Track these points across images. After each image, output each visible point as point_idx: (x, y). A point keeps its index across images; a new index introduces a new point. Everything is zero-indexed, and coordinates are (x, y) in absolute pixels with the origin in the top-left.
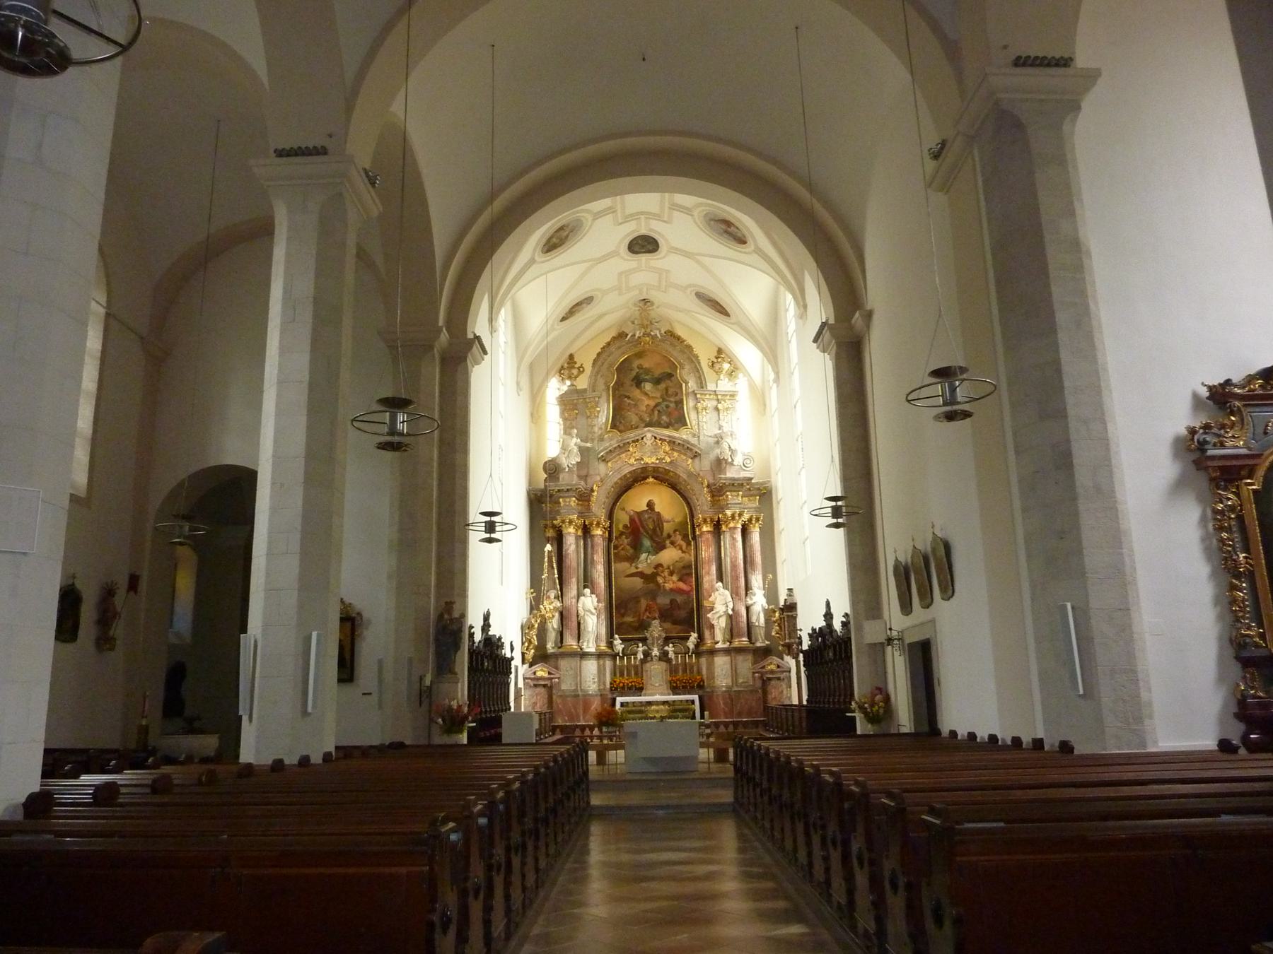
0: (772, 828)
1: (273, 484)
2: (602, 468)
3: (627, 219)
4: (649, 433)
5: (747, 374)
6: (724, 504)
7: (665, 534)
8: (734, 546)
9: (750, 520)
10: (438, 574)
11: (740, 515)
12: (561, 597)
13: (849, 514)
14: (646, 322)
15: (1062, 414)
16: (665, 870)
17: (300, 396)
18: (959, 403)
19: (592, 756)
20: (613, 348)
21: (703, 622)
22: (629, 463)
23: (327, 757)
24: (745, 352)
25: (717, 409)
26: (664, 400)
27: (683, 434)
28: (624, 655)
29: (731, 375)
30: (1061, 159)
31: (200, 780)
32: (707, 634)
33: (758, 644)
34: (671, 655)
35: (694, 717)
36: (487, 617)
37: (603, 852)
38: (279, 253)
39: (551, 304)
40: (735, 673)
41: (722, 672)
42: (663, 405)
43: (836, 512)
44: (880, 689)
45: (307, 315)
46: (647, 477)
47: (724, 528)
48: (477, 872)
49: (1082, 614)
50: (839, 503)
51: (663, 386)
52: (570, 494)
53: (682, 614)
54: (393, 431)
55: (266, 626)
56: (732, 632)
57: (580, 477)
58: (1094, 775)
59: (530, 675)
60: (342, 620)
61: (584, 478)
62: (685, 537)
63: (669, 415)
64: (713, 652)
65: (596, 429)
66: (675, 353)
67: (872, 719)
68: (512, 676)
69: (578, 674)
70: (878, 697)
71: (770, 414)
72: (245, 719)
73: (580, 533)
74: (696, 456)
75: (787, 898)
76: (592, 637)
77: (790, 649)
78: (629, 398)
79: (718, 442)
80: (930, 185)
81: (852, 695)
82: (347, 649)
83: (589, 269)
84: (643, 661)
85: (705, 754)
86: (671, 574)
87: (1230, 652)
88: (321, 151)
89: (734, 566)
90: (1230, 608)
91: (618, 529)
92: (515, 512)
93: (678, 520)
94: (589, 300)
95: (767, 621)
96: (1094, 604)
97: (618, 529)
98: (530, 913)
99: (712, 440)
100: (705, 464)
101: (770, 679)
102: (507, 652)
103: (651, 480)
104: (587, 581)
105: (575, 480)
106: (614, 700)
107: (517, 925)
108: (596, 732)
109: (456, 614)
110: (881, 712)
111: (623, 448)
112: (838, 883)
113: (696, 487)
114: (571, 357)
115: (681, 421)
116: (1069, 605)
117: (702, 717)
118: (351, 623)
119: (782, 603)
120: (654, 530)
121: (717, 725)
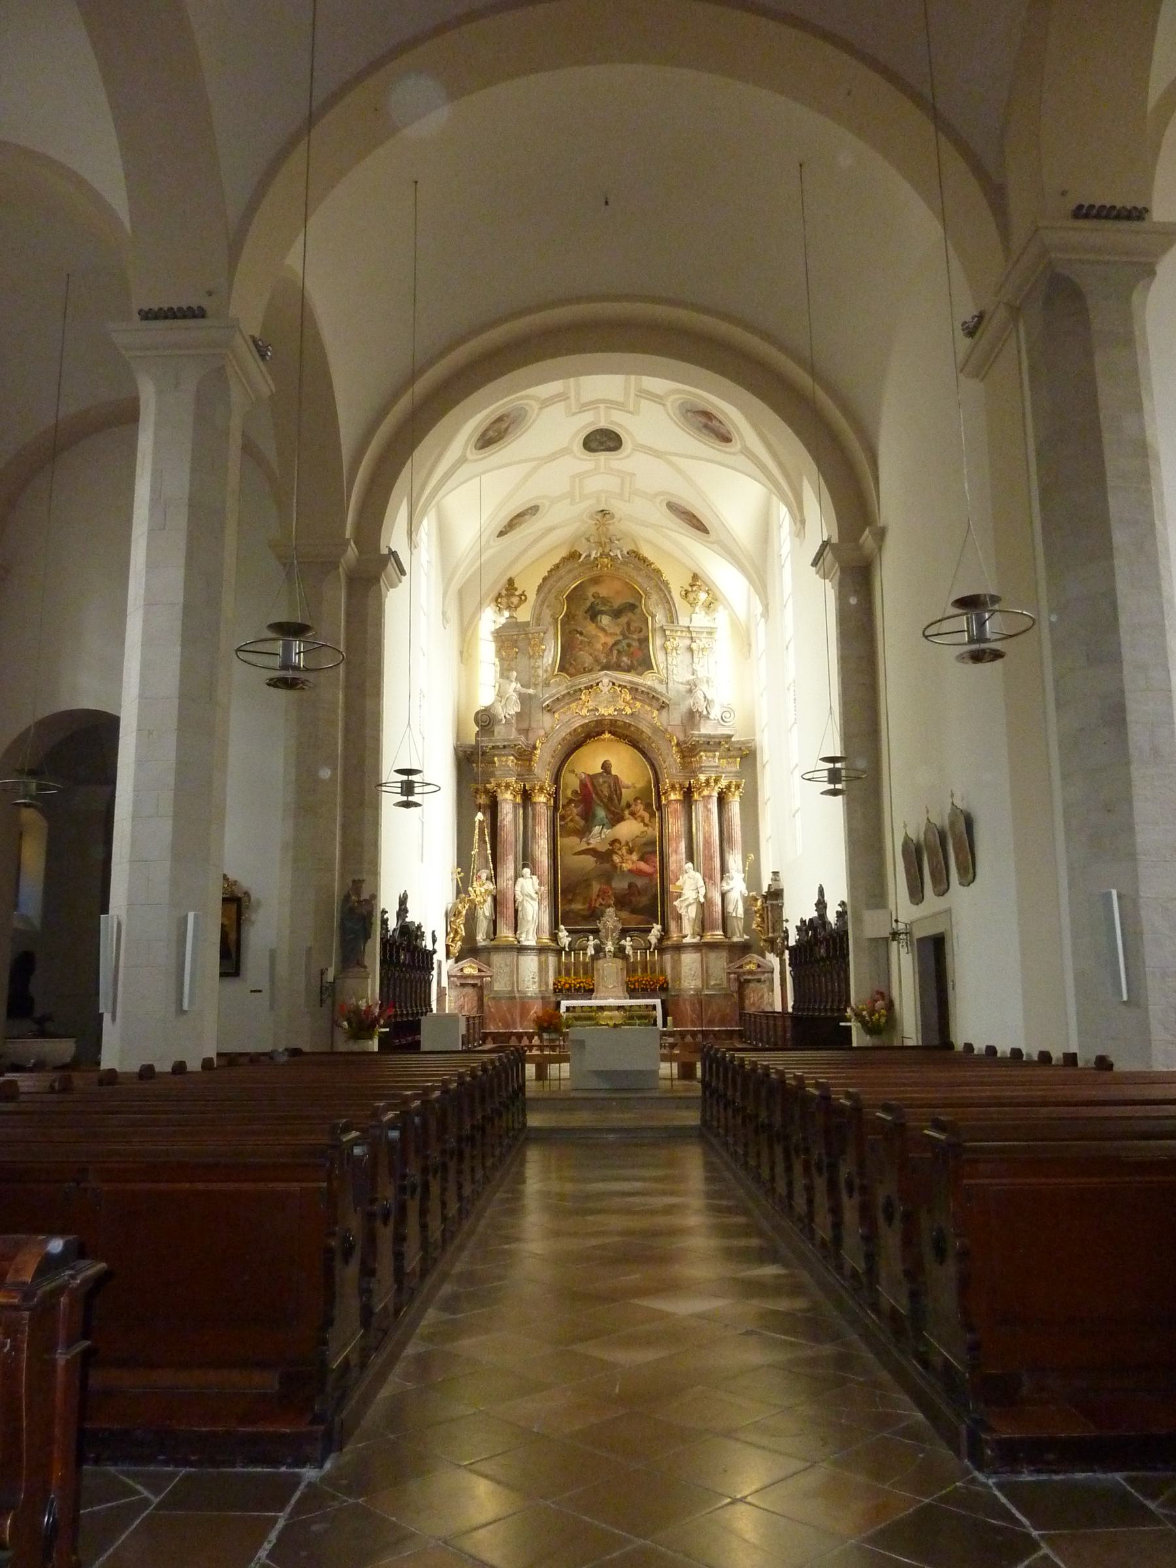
0: (746, 1155)
1: (139, 730)
2: (547, 721)
3: (584, 407)
4: (605, 678)
5: (728, 606)
6: (693, 766)
7: (623, 803)
8: (707, 819)
9: (728, 787)
10: (344, 846)
11: (717, 781)
12: (494, 877)
13: (849, 779)
14: (603, 539)
15: (1115, 659)
16: (617, 1202)
17: (171, 620)
18: (987, 640)
19: (530, 1070)
20: (562, 572)
21: (669, 911)
22: (580, 714)
23: (207, 1064)
24: (723, 575)
25: (690, 649)
26: (625, 637)
27: (648, 680)
28: (571, 950)
29: (708, 606)
30: (1127, 338)
31: (52, 1087)
32: (673, 925)
33: (735, 939)
34: (629, 951)
35: (655, 1024)
36: (403, 901)
37: (556, 1234)
38: (146, 441)
39: (484, 518)
40: (706, 973)
41: (690, 972)
42: (624, 643)
43: (834, 776)
44: (881, 994)
45: (180, 520)
46: (603, 732)
47: (696, 796)
48: (387, 1193)
49: (1130, 904)
50: (838, 765)
51: (623, 620)
52: (506, 751)
53: (644, 900)
54: (286, 665)
55: (131, 905)
56: (703, 924)
57: (520, 731)
58: (1133, 1092)
59: (456, 972)
60: (225, 900)
61: (526, 732)
62: (648, 807)
63: (631, 656)
64: (679, 948)
65: (540, 672)
66: (640, 580)
67: (871, 1029)
68: (435, 973)
69: (515, 971)
70: (880, 1004)
71: (756, 658)
72: (107, 1018)
73: (519, 800)
74: (663, 706)
75: (761, 1234)
76: (532, 928)
77: (773, 946)
78: (581, 634)
79: (690, 691)
80: (961, 371)
81: (848, 1000)
82: (233, 936)
83: (535, 470)
84: (594, 958)
85: (667, 1069)
86: (630, 852)
88: (197, 313)
89: (708, 843)
91: (565, 797)
92: (439, 770)
93: (640, 785)
94: (533, 510)
95: (746, 911)
96: (1147, 892)
97: (565, 797)
98: (451, 1248)
99: (683, 688)
100: (672, 719)
101: (748, 981)
102: (428, 943)
103: (607, 735)
104: (527, 859)
105: (514, 734)
106: (558, 1004)
107: (435, 1260)
108: (536, 1041)
109: (365, 896)
110: (882, 1020)
111: (573, 695)
112: (823, 1219)
113: (663, 745)
114: (511, 582)
115: (645, 664)
116: (1114, 893)
117: (665, 1024)
118: (236, 904)
119: (765, 889)
120: (610, 799)
121: (683, 1034)
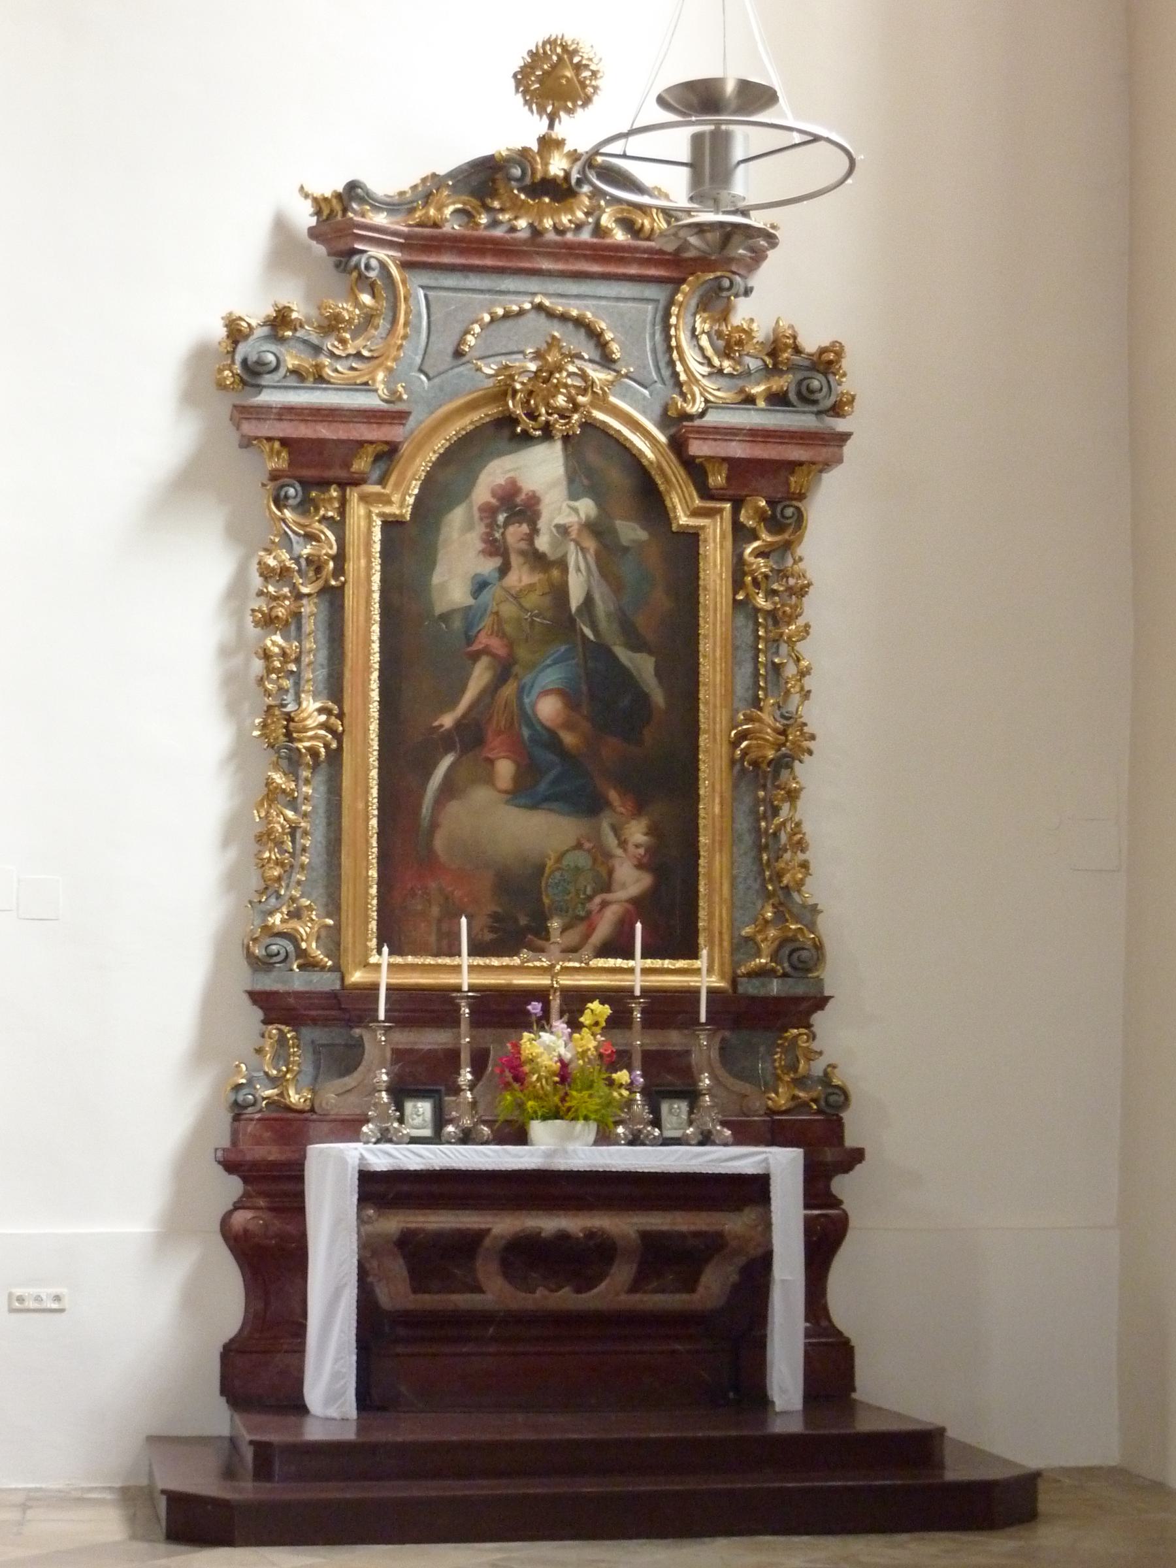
87: (242, 978)
90: (266, 855)
